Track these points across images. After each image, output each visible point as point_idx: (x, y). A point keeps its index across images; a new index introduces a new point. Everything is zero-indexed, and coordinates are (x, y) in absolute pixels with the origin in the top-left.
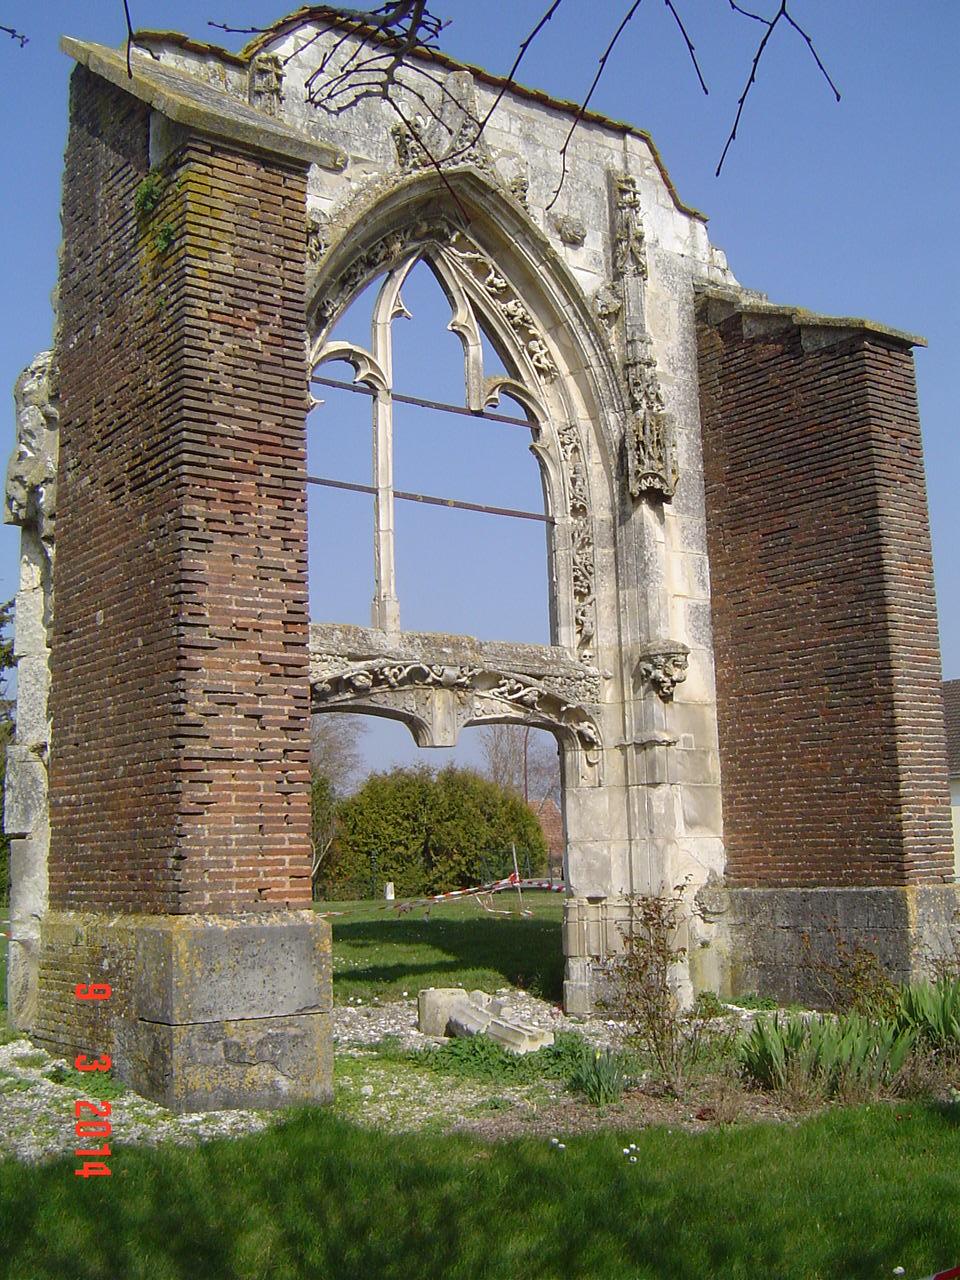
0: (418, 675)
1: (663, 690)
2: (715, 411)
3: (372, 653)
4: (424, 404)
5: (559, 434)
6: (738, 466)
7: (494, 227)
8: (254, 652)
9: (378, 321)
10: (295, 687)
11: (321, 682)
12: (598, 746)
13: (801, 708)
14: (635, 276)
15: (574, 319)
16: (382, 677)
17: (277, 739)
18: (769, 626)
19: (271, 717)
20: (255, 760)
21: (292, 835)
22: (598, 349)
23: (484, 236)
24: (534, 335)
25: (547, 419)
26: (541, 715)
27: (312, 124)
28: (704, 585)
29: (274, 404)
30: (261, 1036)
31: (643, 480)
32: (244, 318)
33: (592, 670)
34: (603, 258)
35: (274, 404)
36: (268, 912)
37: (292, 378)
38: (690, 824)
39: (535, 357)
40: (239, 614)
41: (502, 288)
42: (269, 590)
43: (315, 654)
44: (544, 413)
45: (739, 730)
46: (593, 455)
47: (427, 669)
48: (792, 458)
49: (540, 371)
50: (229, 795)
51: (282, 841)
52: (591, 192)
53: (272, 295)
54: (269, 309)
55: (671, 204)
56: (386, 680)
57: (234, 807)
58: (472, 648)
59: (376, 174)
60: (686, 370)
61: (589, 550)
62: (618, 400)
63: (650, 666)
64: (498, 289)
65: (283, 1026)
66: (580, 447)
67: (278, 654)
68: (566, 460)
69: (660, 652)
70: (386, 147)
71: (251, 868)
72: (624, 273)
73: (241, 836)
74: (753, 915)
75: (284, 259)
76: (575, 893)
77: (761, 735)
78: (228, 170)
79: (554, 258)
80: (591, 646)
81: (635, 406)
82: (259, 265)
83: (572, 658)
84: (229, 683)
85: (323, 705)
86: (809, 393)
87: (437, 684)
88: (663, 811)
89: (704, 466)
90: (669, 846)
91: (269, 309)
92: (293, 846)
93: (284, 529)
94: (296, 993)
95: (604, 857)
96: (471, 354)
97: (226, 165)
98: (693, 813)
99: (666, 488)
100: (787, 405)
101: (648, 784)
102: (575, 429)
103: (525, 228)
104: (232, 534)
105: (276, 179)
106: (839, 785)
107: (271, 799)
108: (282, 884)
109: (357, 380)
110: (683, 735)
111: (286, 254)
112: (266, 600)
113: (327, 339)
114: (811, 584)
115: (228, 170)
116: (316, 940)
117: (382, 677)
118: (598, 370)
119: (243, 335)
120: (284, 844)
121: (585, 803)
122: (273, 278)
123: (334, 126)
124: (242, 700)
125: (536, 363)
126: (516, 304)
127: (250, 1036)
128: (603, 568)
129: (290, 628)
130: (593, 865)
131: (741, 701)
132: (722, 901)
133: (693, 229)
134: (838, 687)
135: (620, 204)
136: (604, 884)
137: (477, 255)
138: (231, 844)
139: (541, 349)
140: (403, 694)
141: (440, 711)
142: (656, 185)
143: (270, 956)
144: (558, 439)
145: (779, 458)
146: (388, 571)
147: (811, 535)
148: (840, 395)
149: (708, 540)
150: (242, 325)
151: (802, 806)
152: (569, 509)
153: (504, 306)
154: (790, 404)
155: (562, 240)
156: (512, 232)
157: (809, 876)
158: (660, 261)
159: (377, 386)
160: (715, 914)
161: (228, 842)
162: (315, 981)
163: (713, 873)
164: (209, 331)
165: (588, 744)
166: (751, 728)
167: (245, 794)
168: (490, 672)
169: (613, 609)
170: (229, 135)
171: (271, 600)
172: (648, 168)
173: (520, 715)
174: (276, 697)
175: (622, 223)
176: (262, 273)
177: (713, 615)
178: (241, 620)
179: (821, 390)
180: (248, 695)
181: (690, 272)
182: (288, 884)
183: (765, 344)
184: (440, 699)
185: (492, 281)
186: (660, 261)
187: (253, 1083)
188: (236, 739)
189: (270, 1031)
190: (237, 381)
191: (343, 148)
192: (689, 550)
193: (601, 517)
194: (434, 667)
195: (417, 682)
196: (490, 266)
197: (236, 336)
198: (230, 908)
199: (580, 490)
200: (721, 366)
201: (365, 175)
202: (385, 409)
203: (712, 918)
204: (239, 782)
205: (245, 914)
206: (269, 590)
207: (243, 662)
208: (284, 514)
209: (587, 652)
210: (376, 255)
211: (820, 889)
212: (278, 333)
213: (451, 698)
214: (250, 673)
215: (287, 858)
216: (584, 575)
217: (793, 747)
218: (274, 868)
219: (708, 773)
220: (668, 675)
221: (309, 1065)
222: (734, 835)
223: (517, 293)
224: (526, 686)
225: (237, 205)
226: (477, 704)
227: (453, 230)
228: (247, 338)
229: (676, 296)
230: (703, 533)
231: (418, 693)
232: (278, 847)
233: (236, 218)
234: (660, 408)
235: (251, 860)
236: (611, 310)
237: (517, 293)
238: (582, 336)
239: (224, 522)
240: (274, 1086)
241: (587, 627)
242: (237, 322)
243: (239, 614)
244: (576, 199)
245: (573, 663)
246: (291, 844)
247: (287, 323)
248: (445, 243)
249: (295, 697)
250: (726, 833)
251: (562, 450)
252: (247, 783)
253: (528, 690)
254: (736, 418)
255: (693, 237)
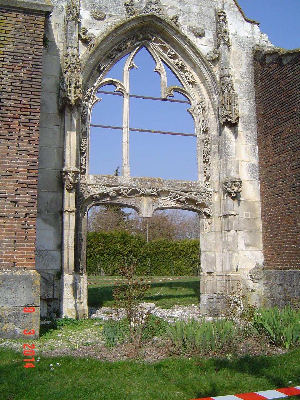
0: (135, 192)
1: (236, 197)
2: (259, 92)
3: (116, 184)
4: (144, 98)
5: (198, 105)
6: (266, 111)
7: (167, 33)
8: (15, 180)
9: (124, 70)
10: (31, 192)
11: (96, 195)
12: (212, 217)
13: (284, 201)
14: (224, 45)
15: (200, 63)
16: (121, 193)
17: (23, 210)
18: (275, 170)
19: (21, 202)
20: (14, 217)
21: (27, 244)
22: (209, 72)
23: (165, 37)
24: (186, 70)
25: (193, 100)
26: (188, 206)
27: (93, 5)
28: (256, 157)
29: (28, 94)
30: (10, 313)
31: (224, 119)
32: (17, 66)
33: (209, 189)
34: (213, 40)
35: (28, 94)
36: (17, 270)
37: (35, 85)
38: (247, 245)
39: (187, 78)
40: (10, 167)
41: (173, 55)
42: (22, 158)
43: (93, 185)
44: (192, 98)
45: (267, 210)
46: (211, 111)
47: (138, 190)
48: (281, 106)
49: (190, 83)
50: (3, 229)
51: (24, 246)
52: (208, 18)
53: (28, 57)
54: (27, 62)
55: (243, 19)
56: (122, 194)
57: (4, 233)
58: (160, 182)
59: (118, 19)
60: (249, 78)
61: (209, 146)
62: (217, 91)
63: (226, 187)
64: (171, 55)
65: (19, 310)
66: (205, 109)
67: (24, 180)
68: (200, 114)
69: (229, 181)
70: (122, 10)
71: (11, 255)
72: (220, 45)
73: (7, 243)
74: (270, 280)
75: (34, 45)
76: (203, 270)
77: (273, 212)
78: (13, 17)
79: (189, 42)
80: (210, 181)
81: (223, 92)
82: (24, 48)
83: (202, 185)
84: (4, 191)
85: (98, 202)
86: (285, 80)
87: (143, 195)
88: (232, 240)
89: (256, 113)
90: (234, 254)
91: (27, 62)
92: (28, 248)
93: (30, 137)
94: (25, 299)
95: (213, 257)
96: (162, 79)
97: (12, 15)
98: (248, 241)
99: (232, 120)
100: (279, 86)
101: (227, 230)
102: (203, 103)
103: (178, 33)
104: (8, 140)
105: (32, 18)
106: (296, 230)
107: (19, 231)
108: (23, 261)
109: (115, 91)
110: (245, 212)
111: (35, 43)
112: (21, 162)
113: (104, 76)
114: (287, 153)
115: (13, 17)
116: (34, 281)
117: (121, 193)
118: (210, 80)
119: (16, 72)
120: (24, 246)
121: (206, 238)
122: (29, 51)
123: (101, 5)
124: (9, 197)
125: (188, 80)
126: (179, 60)
127: (5, 313)
128: (214, 152)
129: (30, 171)
130: (209, 260)
131: (267, 199)
132: (260, 274)
133: (252, 28)
134: (295, 192)
135: (218, 21)
136: (212, 267)
137: (163, 44)
138: (3, 246)
139: (189, 75)
140: (130, 199)
141: (145, 204)
142: (236, 13)
143: (15, 285)
144: (197, 106)
145: (277, 106)
146: (126, 156)
147: (286, 134)
148: (294, 79)
149: (258, 140)
150: (16, 68)
151: (285, 238)
152: (202, 131)
153: (174, 61)
154: (280, 86)
155: (195, 35)
156: (173, 34)
157: (287, 265)
158: (237, 40)
159: (123, 92)
160: (257, 279)
161: (2, 245)
162: (33, 295)
163: (257, 264)
164: (2, 71)
165: (208, 216)
166: (270, 210)
167: (9, 229)
168: (165, 190)
169: (218, 167)
170: (11, 5)
171: (23, 162)
172: (233, 7)
173: (179, 206)
174: (23, 195)
175: (219, 27)
176: (25, 50)
177: (259, 168)
178: (10, 169)
179: (289, 78)
180: (12, 194)
181: (251, 43)
182: (25, 261)
183: (272, 65)
184: (145, 200)
185: (169, 53)
186: (237, 40)
187: (6, 329)
188: (6, 210)
189: (14, 311)
190: (12, 87)
191: (105, 12)
192: (249, 144)
193: (214, 134)
194: (141, 189)
195: (136, 194)
196: (168, 48)
197: (14, 72)
198: (2, 268)
199: (205, 124)
200: (261, 75)
201: (114, 20)
202: (126, 101)
203: (256, 281)
204: (7, 225)
205: (7, 270)
206: (22, 158)
207: (10, 183)
208: (29, 132)
209: (207, 183)
210: (121, 47)
211: (290, 270)
212: (30, 70)
213: (150, 200)
214: (13, 187)
215: (25, 252)
216: (206, 155)
217: (282, 216)
218: (20, 255)
219: (257, 226)
220: (233, 190)
221: (29, 324)
222: (266, 250)
223: (179, 56)
224: (180, 195)
225: (15, 28)
226: (161, 202)
227: (153, 37)
228: (18, 73)
229: (245, 52)
230: (256, 137)
231: (136, 198)
232: (22, 247)
233: (15, 33)
234: (233, 92)
235: (11, 252)
236: (213, 58)
237: (179, 56)
238: (203, 69)
239: (5, 135)
240: (14, 331)
241: (208, 174)
242: (13, 67)
243: (10, 167)
244: (202, 21)
245: (202, 187)
246: (27, 247)
247: (34, 66)
248: (151, 41)
249: (31, 195)
250: (263, 249)
251: (199, 110)
252: (10, 225)
253: (181, 197)
254: (265, 94)
255: (252, 30)
